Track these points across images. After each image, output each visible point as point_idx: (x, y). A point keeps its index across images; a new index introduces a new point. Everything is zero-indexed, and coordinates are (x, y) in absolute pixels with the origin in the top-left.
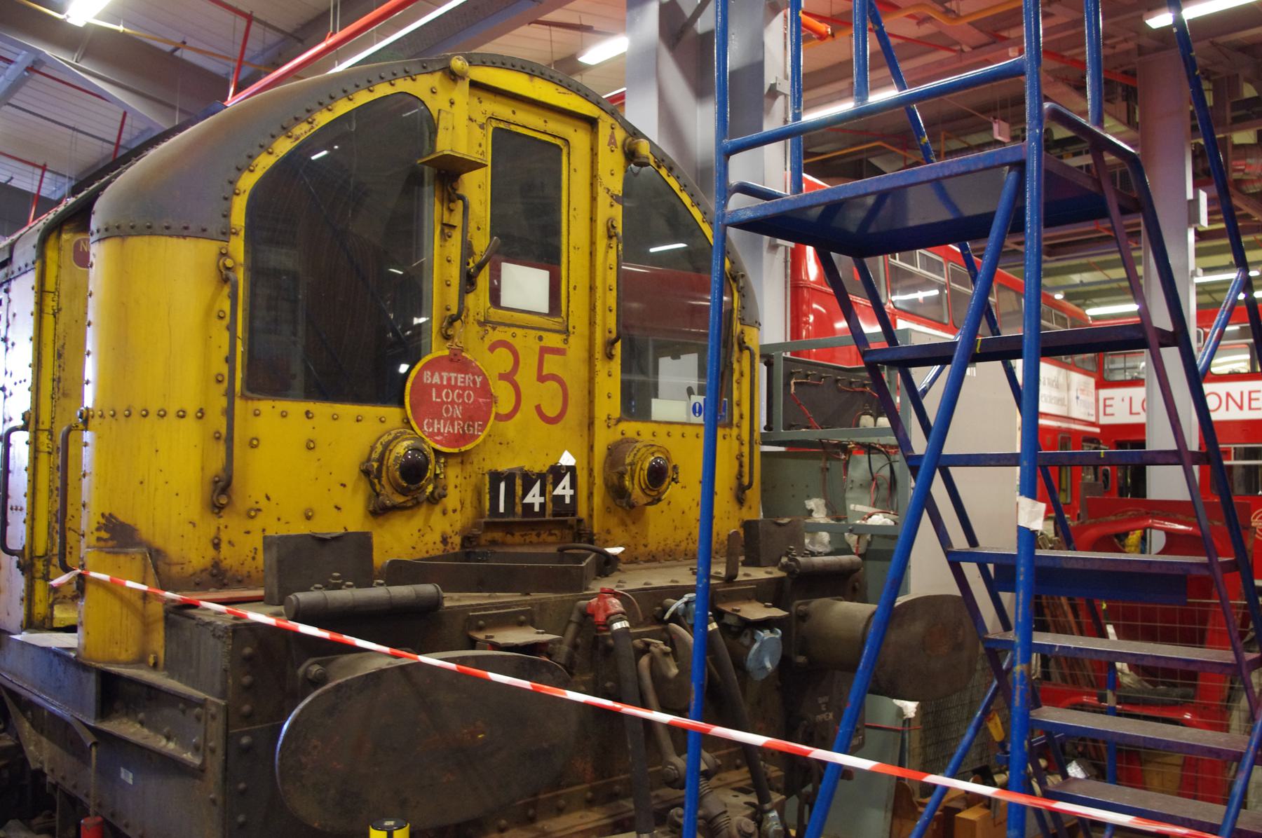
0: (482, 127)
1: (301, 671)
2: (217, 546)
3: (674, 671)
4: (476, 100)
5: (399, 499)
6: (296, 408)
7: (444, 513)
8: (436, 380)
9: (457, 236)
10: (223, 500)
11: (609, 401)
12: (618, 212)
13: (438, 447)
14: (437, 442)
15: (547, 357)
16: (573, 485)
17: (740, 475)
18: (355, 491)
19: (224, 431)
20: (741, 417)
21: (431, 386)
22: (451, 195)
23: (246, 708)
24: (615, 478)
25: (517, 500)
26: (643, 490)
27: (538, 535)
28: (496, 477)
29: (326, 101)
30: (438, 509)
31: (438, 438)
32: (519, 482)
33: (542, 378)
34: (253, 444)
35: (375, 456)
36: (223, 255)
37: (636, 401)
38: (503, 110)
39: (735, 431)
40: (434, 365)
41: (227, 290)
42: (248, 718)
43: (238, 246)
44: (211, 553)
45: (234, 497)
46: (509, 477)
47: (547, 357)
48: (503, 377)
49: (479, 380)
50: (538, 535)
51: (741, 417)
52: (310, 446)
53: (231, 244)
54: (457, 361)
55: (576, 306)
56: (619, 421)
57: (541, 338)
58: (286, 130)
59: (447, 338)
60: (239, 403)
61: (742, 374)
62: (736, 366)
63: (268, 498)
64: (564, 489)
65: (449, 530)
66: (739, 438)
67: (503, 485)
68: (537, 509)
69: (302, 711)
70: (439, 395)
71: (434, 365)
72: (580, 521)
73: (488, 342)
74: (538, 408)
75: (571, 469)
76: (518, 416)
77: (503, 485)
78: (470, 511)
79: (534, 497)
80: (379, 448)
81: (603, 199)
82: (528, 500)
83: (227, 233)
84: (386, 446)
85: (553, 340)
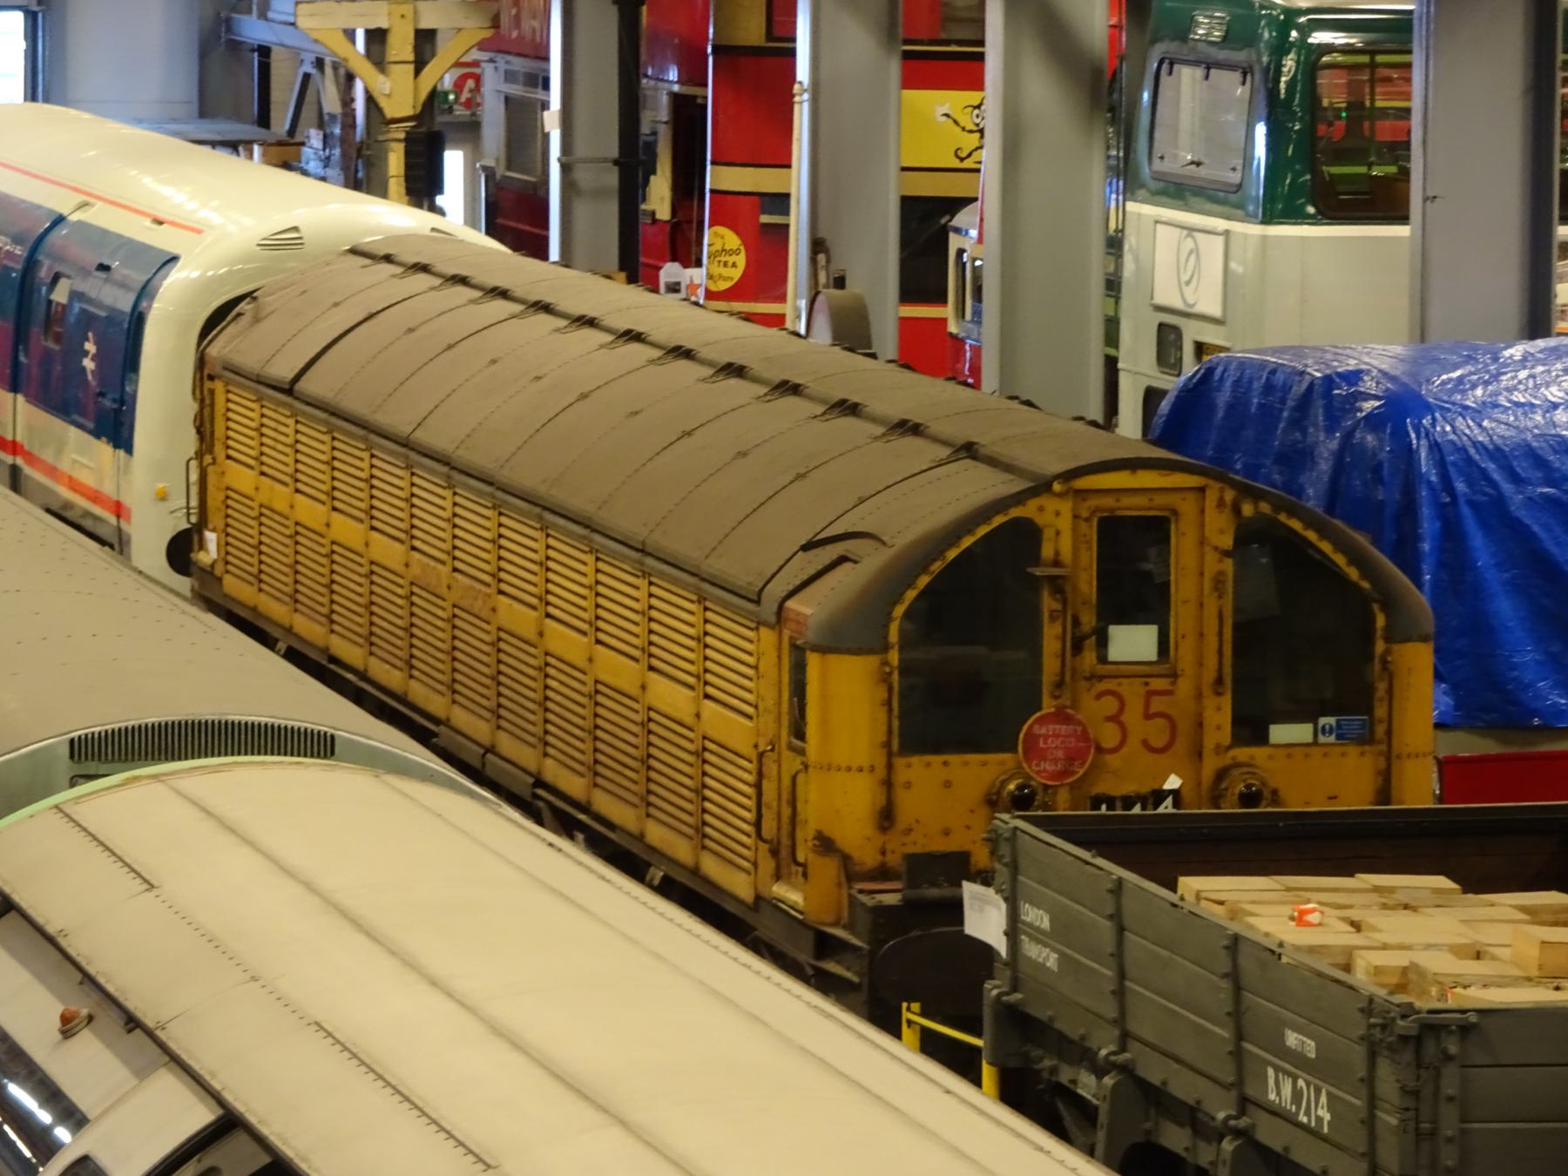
33: (1148, 716)
34: (908, 785)
44: (879, 858)
48: (1109, 719)
56: (1229, 748)
73: (1094, 692)
74: (1145, 743)
76: (1125, 750)
83: (886, 648)
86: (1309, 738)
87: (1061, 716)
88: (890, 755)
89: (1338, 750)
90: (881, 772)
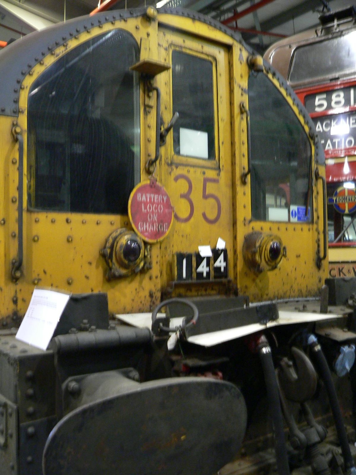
0: (166, 49)
1: (64, 386)
2: (15, 302)
3: (295, 376)
4: (162, 34)
5: (123, 271)
6: (60, 217)
7: (151, 278)
8: (144, 198)
9: (154, 112)
10: (18, 274)
11: (244, 210)
12: (245, 99)
13: (146, 239)
14: (146, 236)
15: (209, 184)
16: (226, 259)
17: (318, 252)
18: (97, 267)
19: (17, 232)
20: (318, 218)
21: (141, 202)
22: (149, 88)
23: (31, 409)
24: (250, 256)
25: (193, 270)
26: (267, 262)
27: (206, 290)
28: (180, 257)
29: (74, 33)
30: (147, 277)
31: (146, 234)
32: (194, 259)
33: (205, 197)
34: (35, 240)
35: (108, 245)
36: (15, 125)
37: (259, 211)
38: (178, 40)
39: (315, 226)
40: (142, 190)
41: (17, 146)
42: (31, 416)
43: (23, 120)
44: (12, 306)
45: (25, 272)
46: (189, 257)
47: (209, 184)
48: (183, 196)
49: (165, 199)
50: (206, 290)
51: (318, 218)
52: (69, 240)
53: (19, 118)
54: (154, 188)
55: (223, 152)
56: (250, 221)
57: (204, 173)
58: (51, 51)
59: (149, 172)
60: (25, 215)
61: (318, 193)
62: (314, 188)
63: (45, 272)
64: (220, 263)
65: (154, 290)
66: (317, 230)
67: (185, 262)
68: (205, 275)
69: (59, 429)
70: (146, 208)
71: (142, 190)
72: (229, 282)
73: (173, 176)
74: (204, 215)
75: (225, 251)
76: (192, 219)
77: (185, 262)
78: (165, 277)
79: (203, 268)
80: (111, 240)
81: (237, 92)
82: (200, 269)
83: (17, 112)
84: (115, 239)
85: (211, 174)
86: (286, 218)
87: (154, 188)
88: (20, 209)
89: (299, 227)
90: (14, 227)
